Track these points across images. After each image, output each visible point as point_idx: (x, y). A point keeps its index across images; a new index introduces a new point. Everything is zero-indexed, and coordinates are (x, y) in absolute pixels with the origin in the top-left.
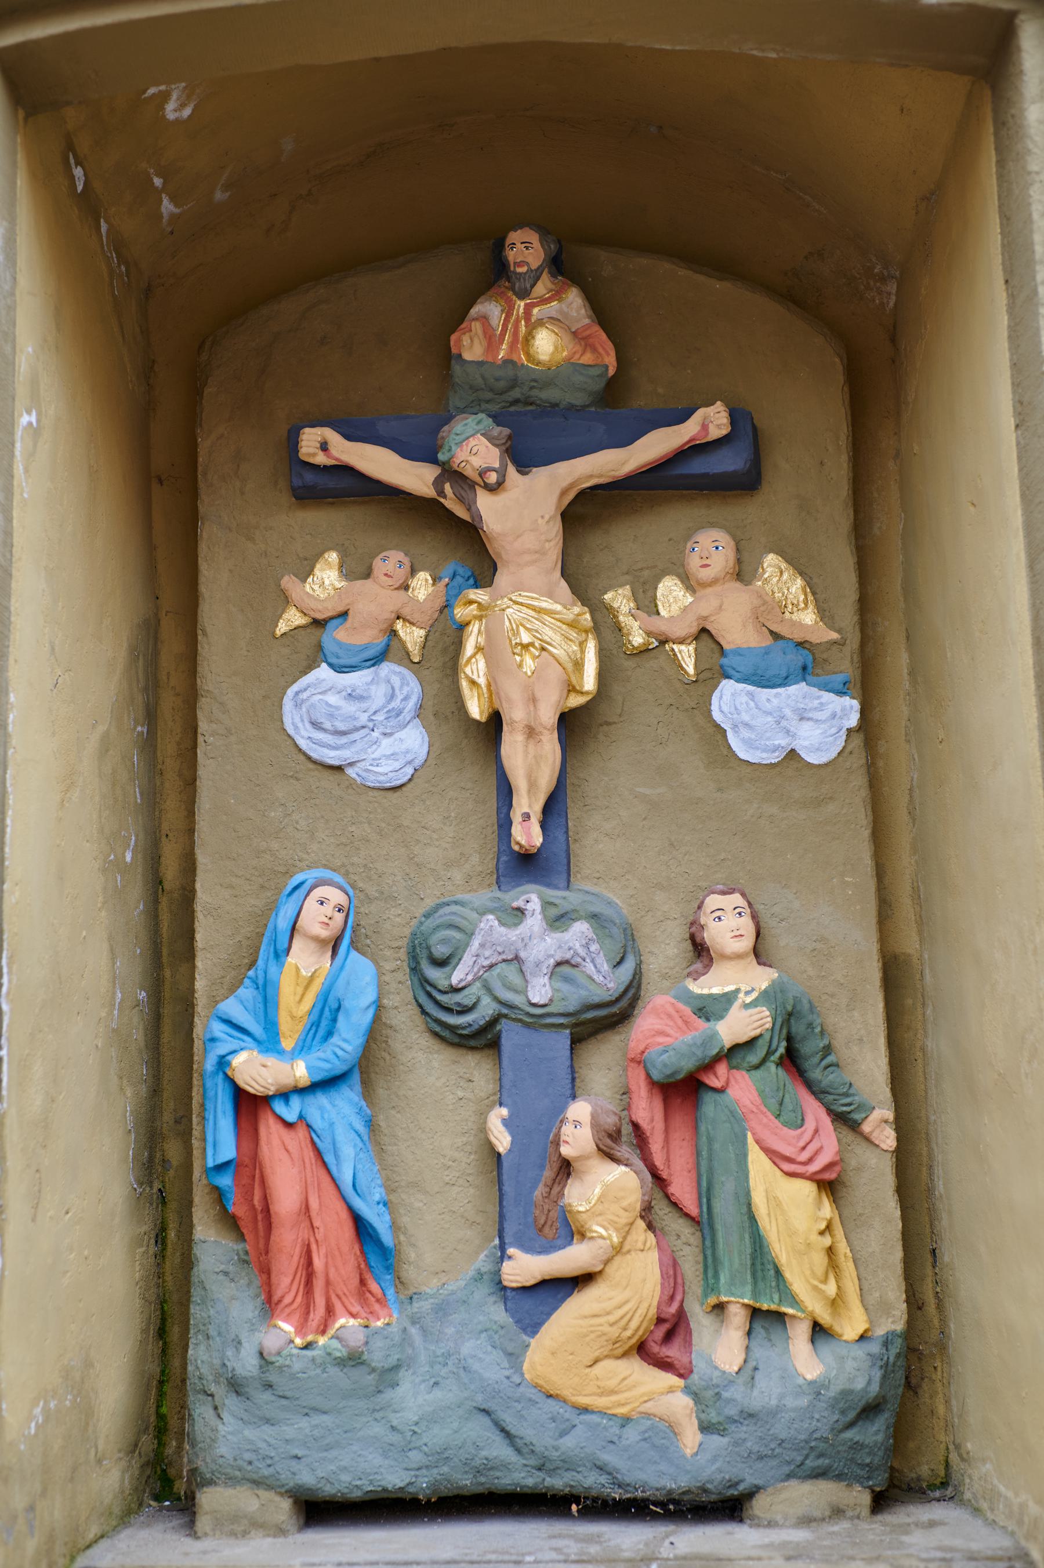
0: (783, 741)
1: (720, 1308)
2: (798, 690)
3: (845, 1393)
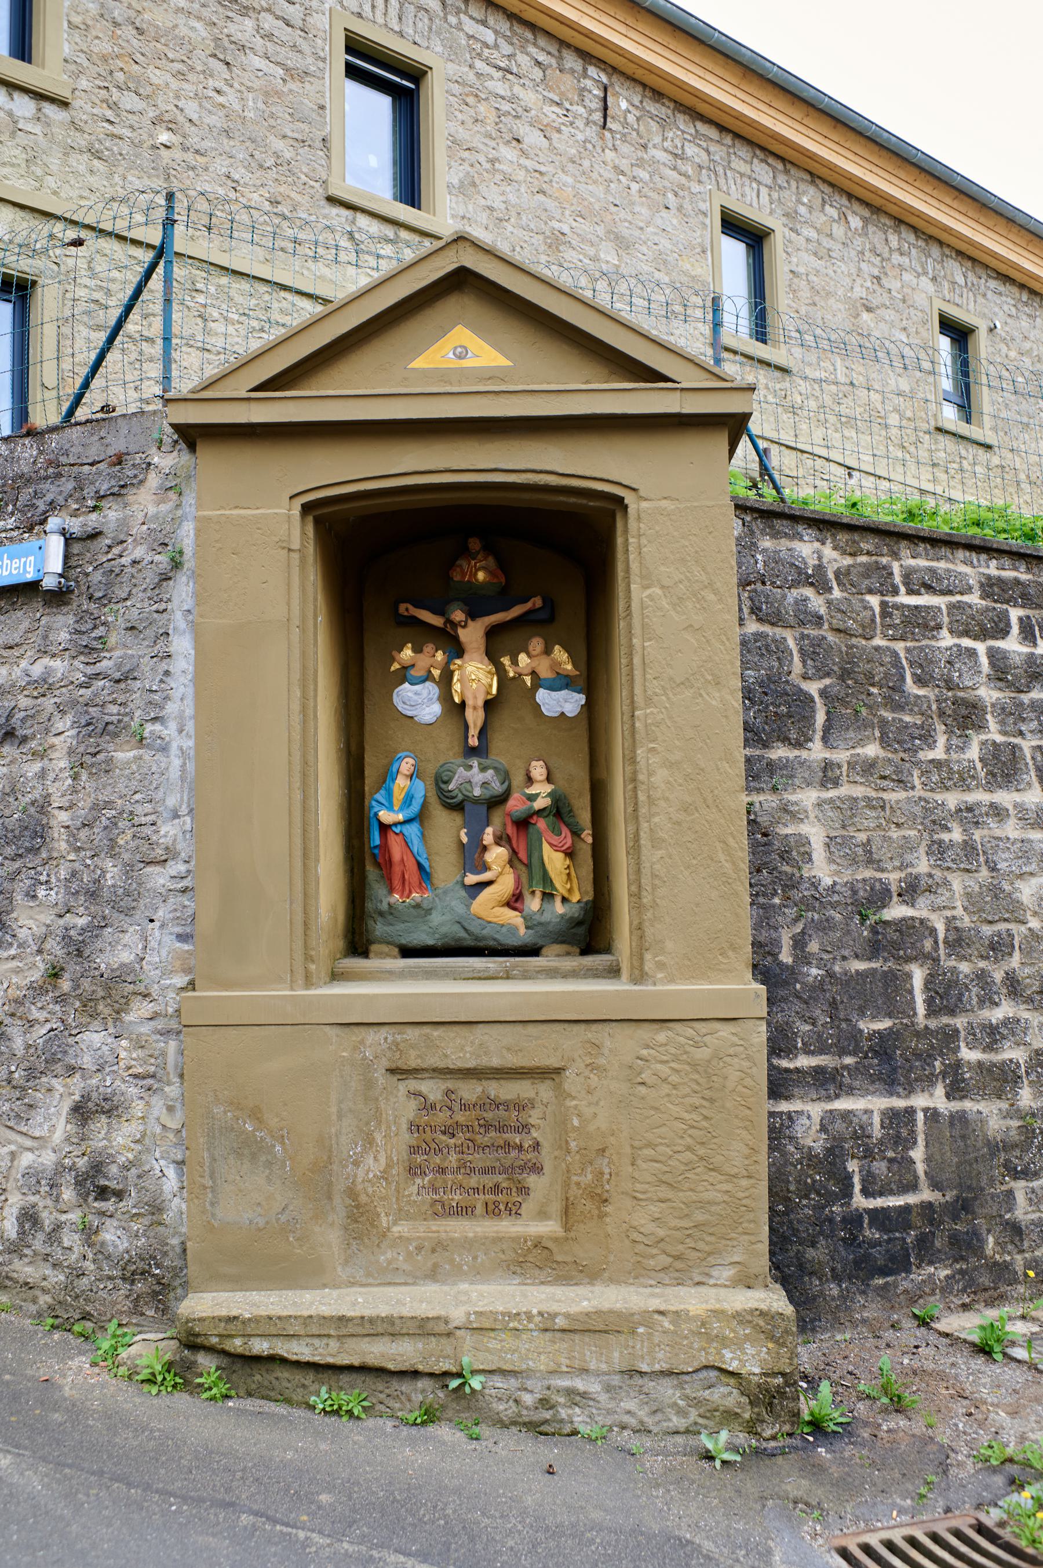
0: (559, 709)
1: (533, 892)
2: (564, 693)
3: (571, 918)
